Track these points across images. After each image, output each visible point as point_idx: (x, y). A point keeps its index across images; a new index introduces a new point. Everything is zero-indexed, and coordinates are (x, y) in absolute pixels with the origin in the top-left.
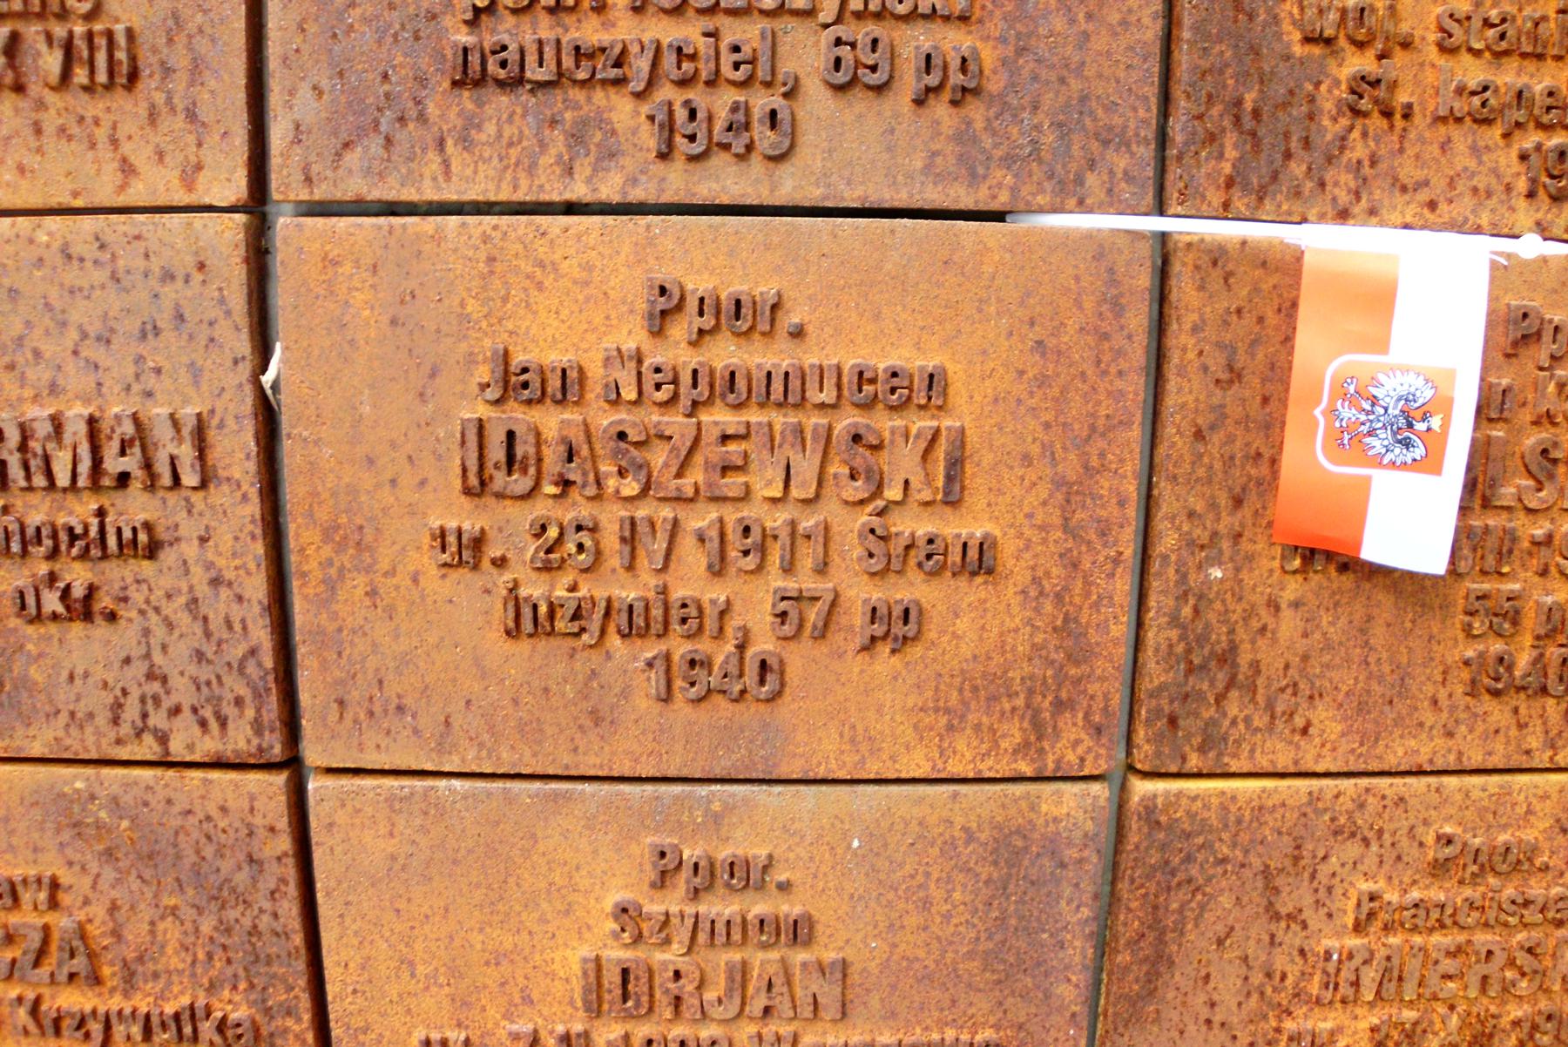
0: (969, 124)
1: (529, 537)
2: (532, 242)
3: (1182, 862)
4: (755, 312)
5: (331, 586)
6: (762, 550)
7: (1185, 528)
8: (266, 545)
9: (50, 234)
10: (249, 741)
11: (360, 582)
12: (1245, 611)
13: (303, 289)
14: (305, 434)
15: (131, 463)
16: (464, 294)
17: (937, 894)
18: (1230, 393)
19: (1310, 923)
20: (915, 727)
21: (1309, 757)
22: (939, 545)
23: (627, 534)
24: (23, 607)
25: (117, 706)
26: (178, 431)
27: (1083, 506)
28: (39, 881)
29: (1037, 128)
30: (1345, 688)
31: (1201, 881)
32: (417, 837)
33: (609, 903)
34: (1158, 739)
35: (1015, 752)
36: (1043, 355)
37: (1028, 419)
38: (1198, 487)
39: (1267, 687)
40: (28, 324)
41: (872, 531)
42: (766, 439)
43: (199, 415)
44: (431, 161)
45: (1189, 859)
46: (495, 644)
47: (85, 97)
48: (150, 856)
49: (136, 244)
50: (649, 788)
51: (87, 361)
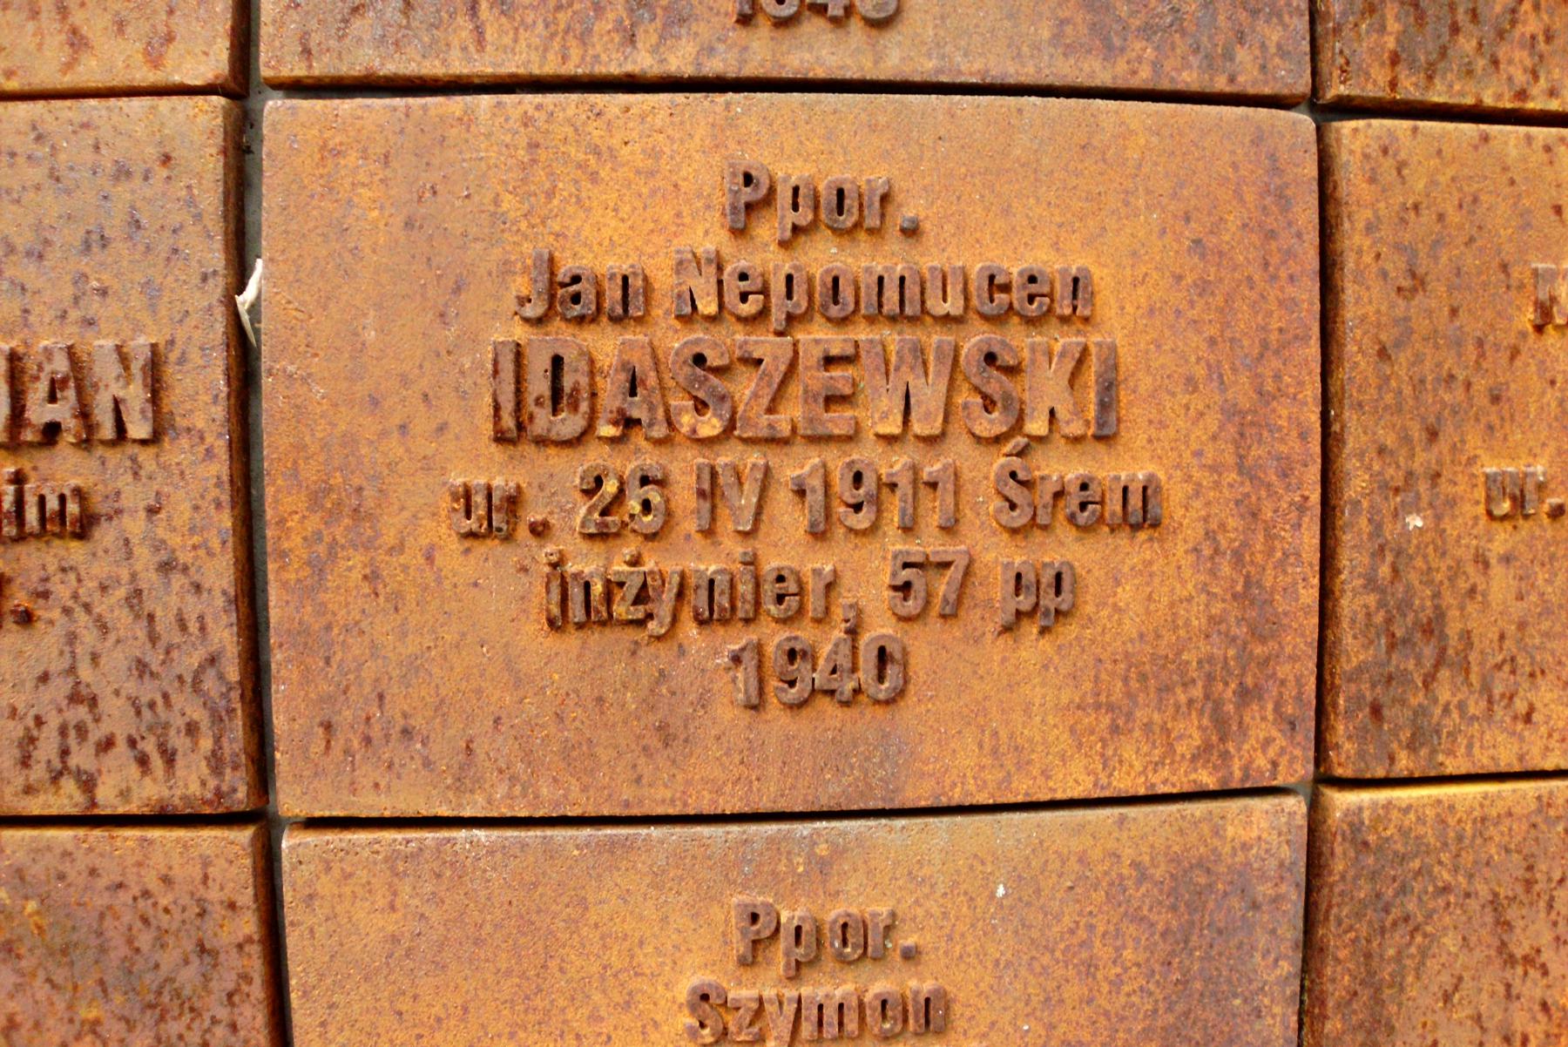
1: (578, 496)
2: (584, 124)
3: (1396, 895)
4: (861, 205)
5: (319, 569)
6: (877, 501)
7: (1376, 467)
10: (203, 784)
11: (356, 562)
12: (1450, 568)
13: (295, 187)
14: (291, 368)
15: (62, 412)
17: (1103, 952)
18: (1414, 303)
19: (1552, 967)
20: (1072, 730)
21: (1536, 751)
22: (1094, 493)
23: (706, 486)
25: (29, 740)
26: (127, 368)
31: (1420, 919)
32: (427, 910)
33: (684, 989)
34: (1360, 735)
35: (1194, 758)
36: (1203, 256)
37: (1190, 334)
41: (1013, 475)
42: (880, 361)
43: (154, 346)
44: (462, 28)
45: (1403, 890)
46: (532, 637)
48: (64, 952)
49: (84, 133)
50: (735, 829)
51: (12, 282)
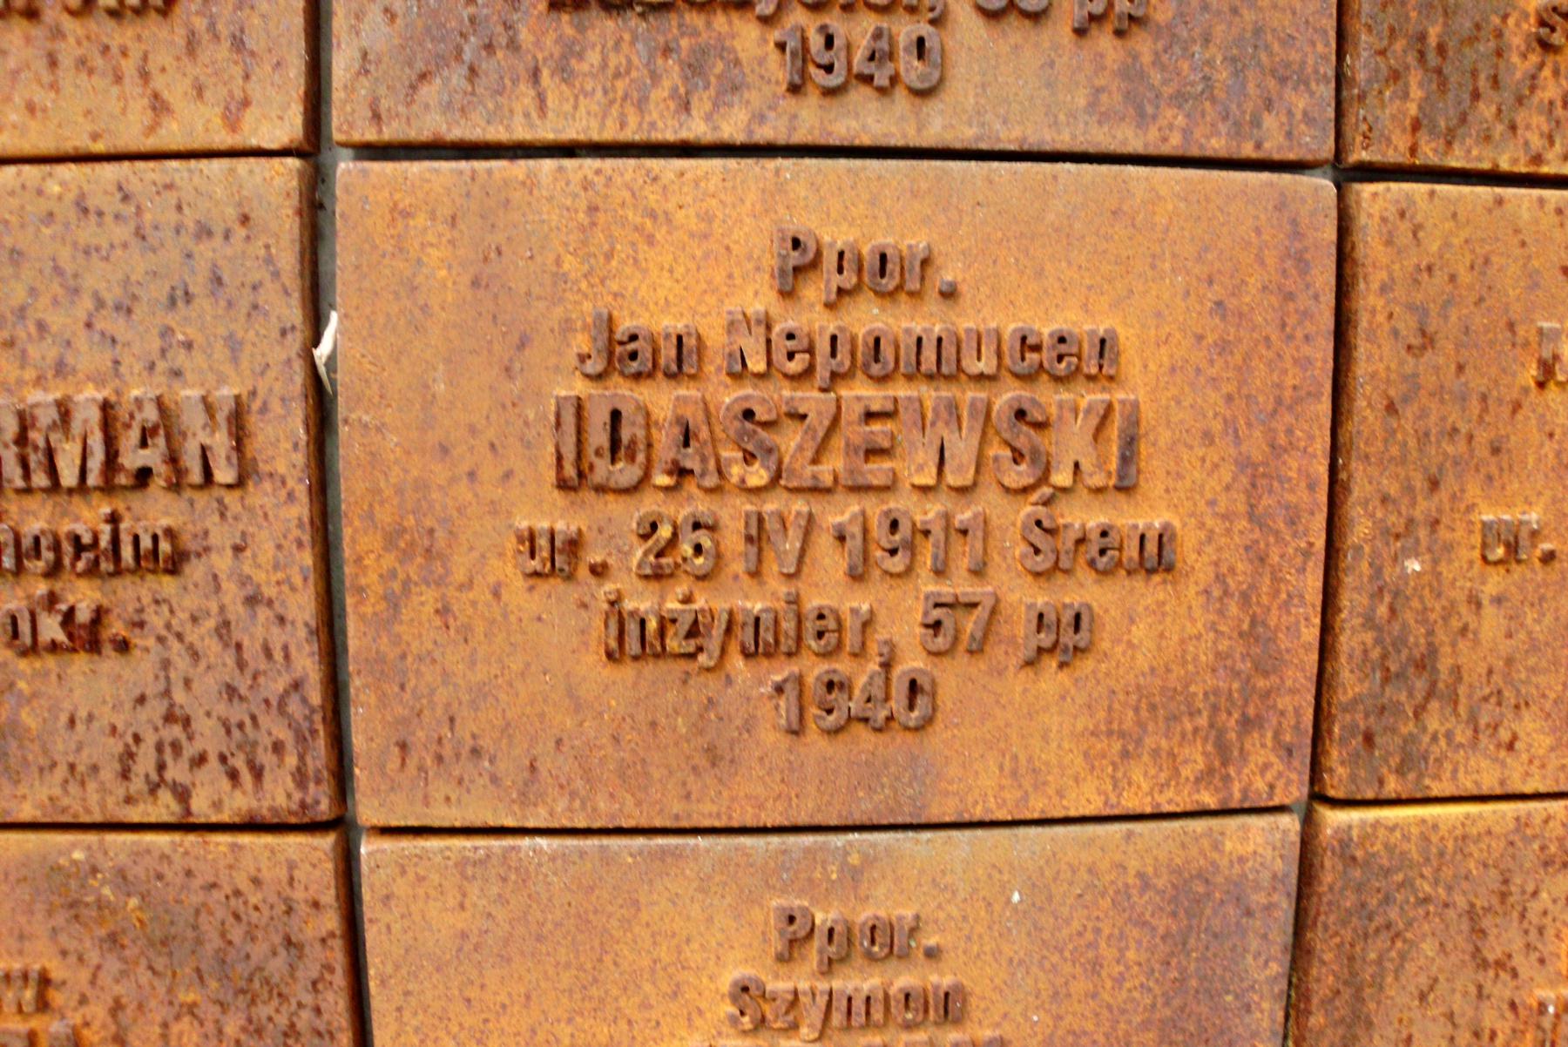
0: (1135, 57)
1: (635, 539)
2: (641, 188)
3: (1380, 904)
4: (902, 268)
5: (394, 603)
6: (911, 547)
7: (1379, 515)
8: (315, 555)
9: (63, 184)
10: (289, 796)
11: (428, 598)
12: (1444, 608)
13: (367, 246)
15: (152, 457)
16: (561, 250)
17: (1108, 952)
20: (1086, 755)
22: (1113, 539)
23: (754, 532)
24: (15, 634)
26: (212, 416)
27: (1270, 491)
28: (25, 977)
29: (1209, 63)
30: (1552, 695)
34: (1353, 760)
35: (1198, 780)
36: (1224, 318)
37: (1209, 391)
38: (1392, 467)
39: (1470, 697)
40: (33, 291)
41: (1039, 523)
43: (237, 398)
45: (1387, 900)
46: (591, 666)
47: (111, 24)
48: (164, 943)
50: (775, 840)
51: (103, 334)
